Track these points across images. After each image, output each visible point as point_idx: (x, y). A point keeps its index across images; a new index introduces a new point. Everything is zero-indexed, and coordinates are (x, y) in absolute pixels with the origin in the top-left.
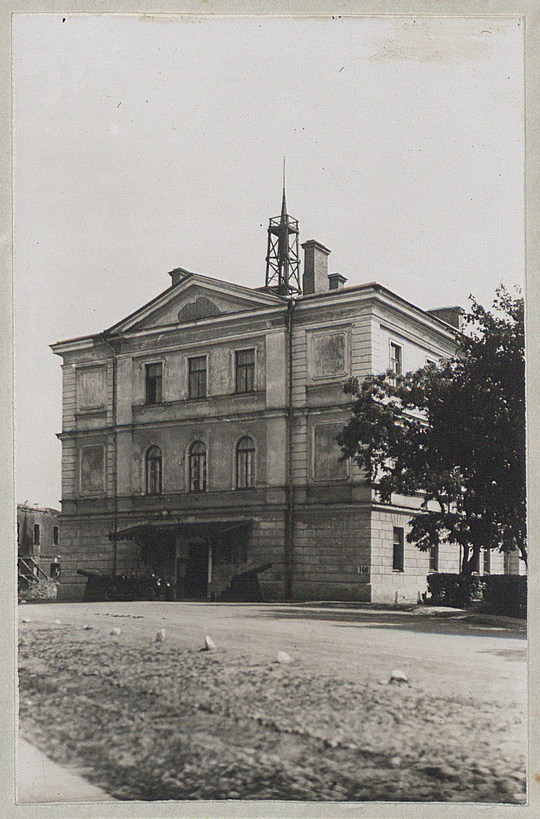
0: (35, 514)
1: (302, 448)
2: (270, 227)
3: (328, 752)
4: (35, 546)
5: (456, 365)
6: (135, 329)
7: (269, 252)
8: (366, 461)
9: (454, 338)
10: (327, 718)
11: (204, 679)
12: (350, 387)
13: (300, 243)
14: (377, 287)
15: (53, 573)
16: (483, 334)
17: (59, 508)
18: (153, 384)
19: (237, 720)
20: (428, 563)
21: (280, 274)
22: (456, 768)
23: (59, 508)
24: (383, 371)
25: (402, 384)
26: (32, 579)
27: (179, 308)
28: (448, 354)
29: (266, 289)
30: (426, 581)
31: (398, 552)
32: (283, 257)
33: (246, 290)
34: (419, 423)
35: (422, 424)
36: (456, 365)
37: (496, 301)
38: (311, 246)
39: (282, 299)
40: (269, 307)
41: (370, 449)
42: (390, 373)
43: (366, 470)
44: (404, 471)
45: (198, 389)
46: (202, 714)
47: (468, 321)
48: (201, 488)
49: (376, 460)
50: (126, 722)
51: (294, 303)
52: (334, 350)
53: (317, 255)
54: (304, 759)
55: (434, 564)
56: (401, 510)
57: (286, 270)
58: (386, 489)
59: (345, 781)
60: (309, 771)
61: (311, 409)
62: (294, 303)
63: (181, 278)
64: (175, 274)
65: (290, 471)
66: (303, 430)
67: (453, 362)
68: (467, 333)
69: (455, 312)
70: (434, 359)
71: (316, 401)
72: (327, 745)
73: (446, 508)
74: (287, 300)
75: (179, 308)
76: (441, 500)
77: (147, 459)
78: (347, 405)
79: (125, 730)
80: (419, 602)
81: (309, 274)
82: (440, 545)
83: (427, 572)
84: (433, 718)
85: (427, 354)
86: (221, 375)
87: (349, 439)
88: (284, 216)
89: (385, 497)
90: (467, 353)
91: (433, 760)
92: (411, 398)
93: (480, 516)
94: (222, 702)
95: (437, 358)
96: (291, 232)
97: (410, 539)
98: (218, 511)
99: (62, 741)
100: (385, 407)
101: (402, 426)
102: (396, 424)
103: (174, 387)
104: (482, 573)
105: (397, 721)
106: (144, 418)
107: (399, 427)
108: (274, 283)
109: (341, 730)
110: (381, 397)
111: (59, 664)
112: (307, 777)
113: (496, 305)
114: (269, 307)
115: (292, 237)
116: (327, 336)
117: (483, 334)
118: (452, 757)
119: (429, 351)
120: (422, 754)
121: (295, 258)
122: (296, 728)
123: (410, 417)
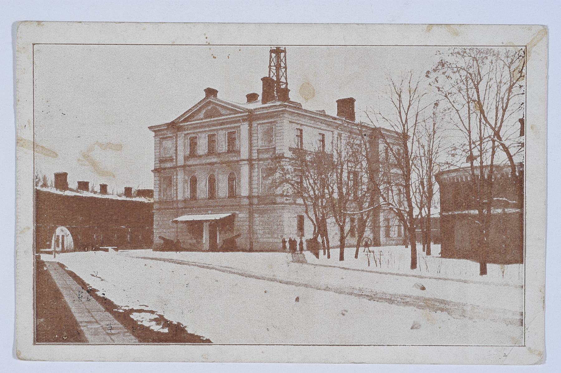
45: (211, 152)
65: (251, 189)
103: (202, 147)
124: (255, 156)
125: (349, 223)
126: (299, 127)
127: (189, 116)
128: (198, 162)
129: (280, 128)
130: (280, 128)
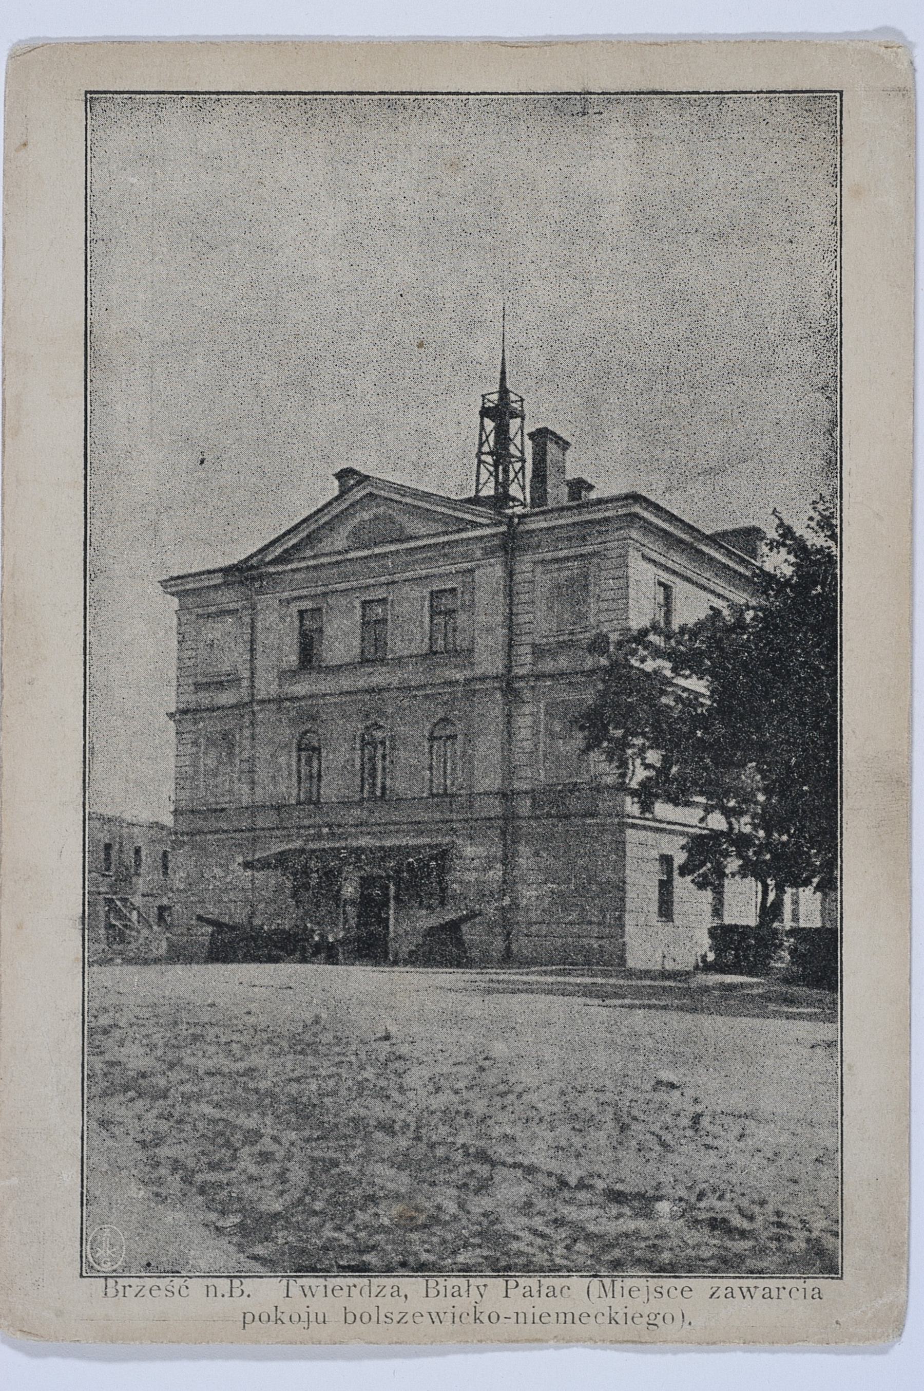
0: (136, 830)
1: (525, 733)
2: (483, 407)
3: (566, 1194)
4: (134, 879)
5: (751, 613)
7: (481, 445)
8: (618, 755)
9: (748, 573)
10: (563, 1143)
11: (382, 1083)
12: (598, 645)
13: (526, 431)
14: (636, 498)
15: (161, 918)
16: (792, 569)
17: (168, 820)
19: (432, 1146)
20: (708, 909)
21: (497, 477)
22: (751, 1218)
23: (168, 820)
24: (646, 622)
25: (673, 642)
26: (132, 929)
28: (740, 598)
29: (476, 500)
30: (707, 935)
31: (666, 887)
32: (501, 455)
33: (446, 501)
34: (696, 699)
35: (701, 700)
36: (751, 613)
37: (811, 519)
38: (541, 436)
39: (500, 513)
40: (482, 525)
41: (624, 737)
42: (655, 628)
43: (618, 768)
44: (674, 769)
45: (373, 653)
46: (379, 1135)
47: (771, 550)
48: (378, 794)
49: (635, 754)
50: (266, 1144)
51: (516, 520)
53: (552, 449)
54: (529, 1204)
55: (717, 912)
56: (669, 827)
57: (506, 471)
58: (646, 795)
59: (589, 1237)
60: (538, 1223)
61: (539, 677)
62: (516, 520)
63: (352, 482)
64: (342, 475)
67: (748, 608)
68: (768, 567)
69: (751, 535)
70: (719, 604)
71: (548, 666)
72: (563, 1183)
73: (736, 826)
74: (506, 516)
76: (728, 813)
77: (299, 750)
78: (593, 672)
79: (265, 1157)
80: (697, 967)
81: (540, 475)
82: (726, 882)
83: (709, 921)
84: (716, 1143)
85: (710, 596)
86: (410, 633)
87: (593, 725)
88: (504, 392)
89: (646, 807)
90: (768, 595)
91: (718, 1204)
92: (683, 662)
93: (785, 838)
94: (409, 1119)
95: (725, 604)
96: (514, 415)
97: (684, 870)
99: (175, 1170)
100: (647, 675)
101: (672, 704)
102: (664, 700)
103: (341, 638)
104: (788, 924)
105: (664, 1145)
107: (667, 706)
108: (488, 491)
109: (582, 1161)
110: (643, 660)
111: (170, 1057)
112: (535, 1232)
113: (813, 524)
114: (482, 525)
115: (514, 424)
117: (792, 569)
118: (745, 1203)
119: (712, 592)
120: (701, 1196)
121: (519, 455)
122: (520, 1158)
123: (685, 690)
124: (525, 663)
125: (774, 891)
126: (665, 577)
127: (310, 532)
128: (326, 685)
129: (527, 618)
130: (527, 618)
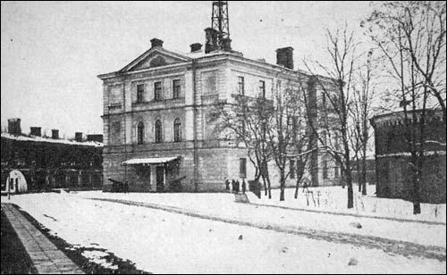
6: (132, 69)
18: (140, 91)
27: (151, 60)
52: (212, 81)
65: (196, 133)
66: (200, 116)
75: (151, 60)
98: (253, 64)
103: (149, 94)
106: (138, 109)
116: (209, 75)
